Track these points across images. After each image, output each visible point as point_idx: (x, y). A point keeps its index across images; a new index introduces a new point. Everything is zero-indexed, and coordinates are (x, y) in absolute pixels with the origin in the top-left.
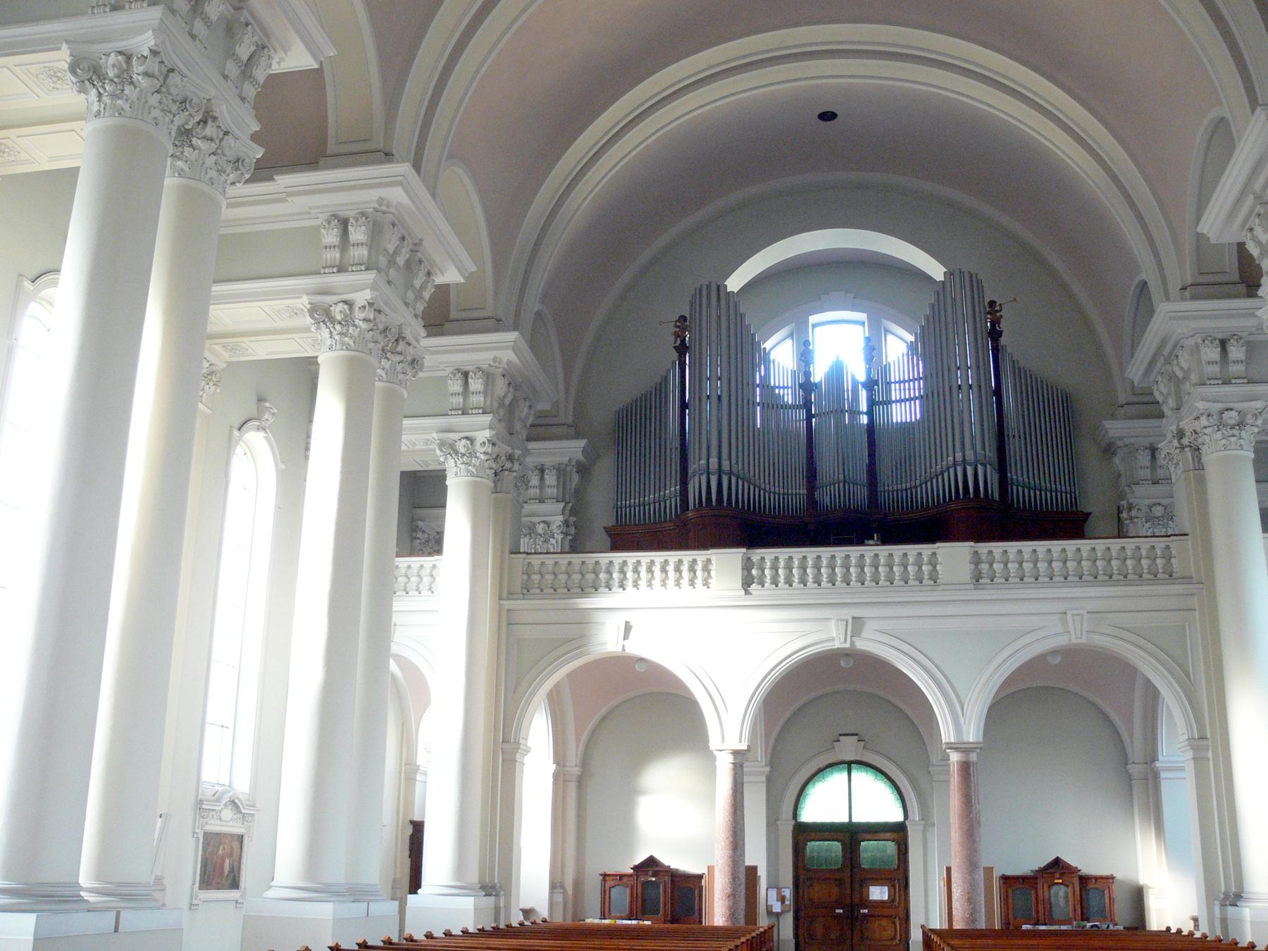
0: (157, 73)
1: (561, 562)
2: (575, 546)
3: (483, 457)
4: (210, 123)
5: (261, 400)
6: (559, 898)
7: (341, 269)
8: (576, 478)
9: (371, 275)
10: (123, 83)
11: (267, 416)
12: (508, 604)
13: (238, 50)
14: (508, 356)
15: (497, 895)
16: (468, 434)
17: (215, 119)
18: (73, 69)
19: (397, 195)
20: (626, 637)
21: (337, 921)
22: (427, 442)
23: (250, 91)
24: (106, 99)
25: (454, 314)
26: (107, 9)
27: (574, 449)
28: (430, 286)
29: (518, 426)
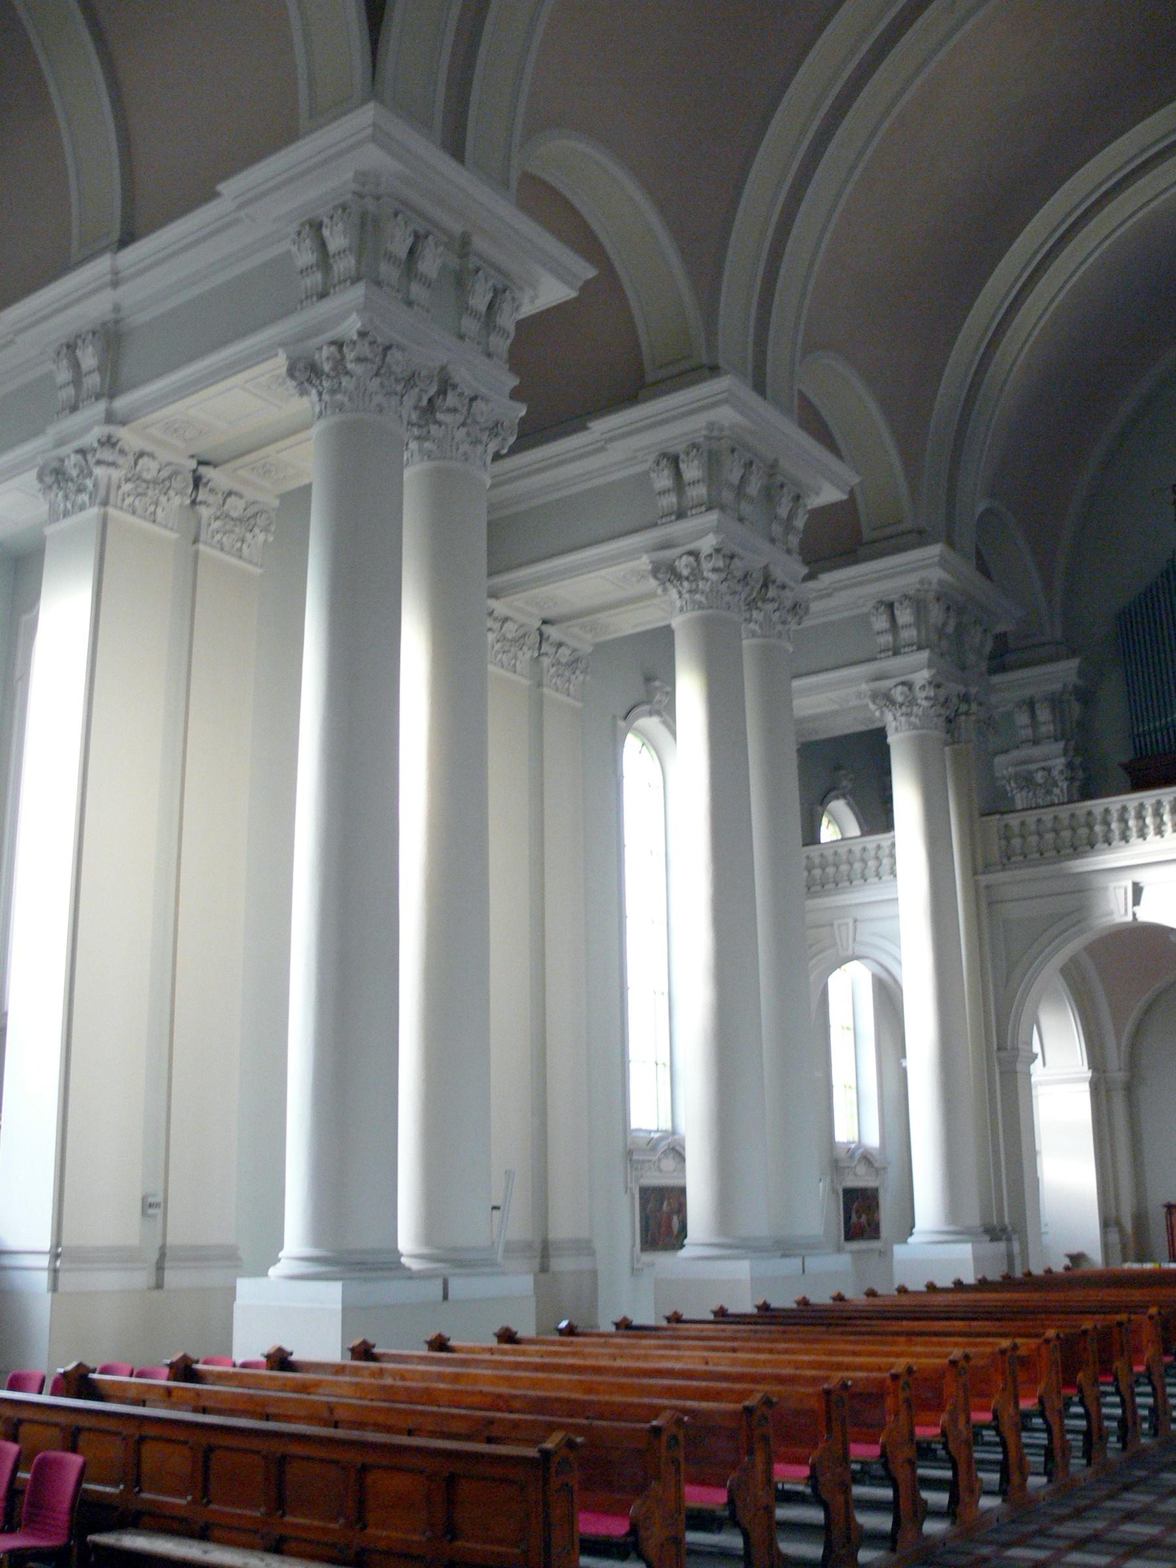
0: (370, 356)
1: (1044, 818)
2: (1088, 792)
3: (925, 703)
4: (450, 394)
5: (648, 679)
6: (1114, 1237)
7: (681, 515)
8: (1076, 709)
9: (713, 517)
10: (337, 375)
11: (658, 697)
12: (984, 879)
13: (472, 302)
14: (936, 575)
15: (1009, 1240)
16: (903, 679)
17: (455, 387)
18: (291, 373)
19: (726, 415)
20: (1137, 901)
21: (755, 1281)
22: (859, 695)
23: (501, 345)
24: (326, 397)
25: (867, 535)
26: (315, 298)
27: (1063, 673)
28: (801, 511)
29: (972, 658)
